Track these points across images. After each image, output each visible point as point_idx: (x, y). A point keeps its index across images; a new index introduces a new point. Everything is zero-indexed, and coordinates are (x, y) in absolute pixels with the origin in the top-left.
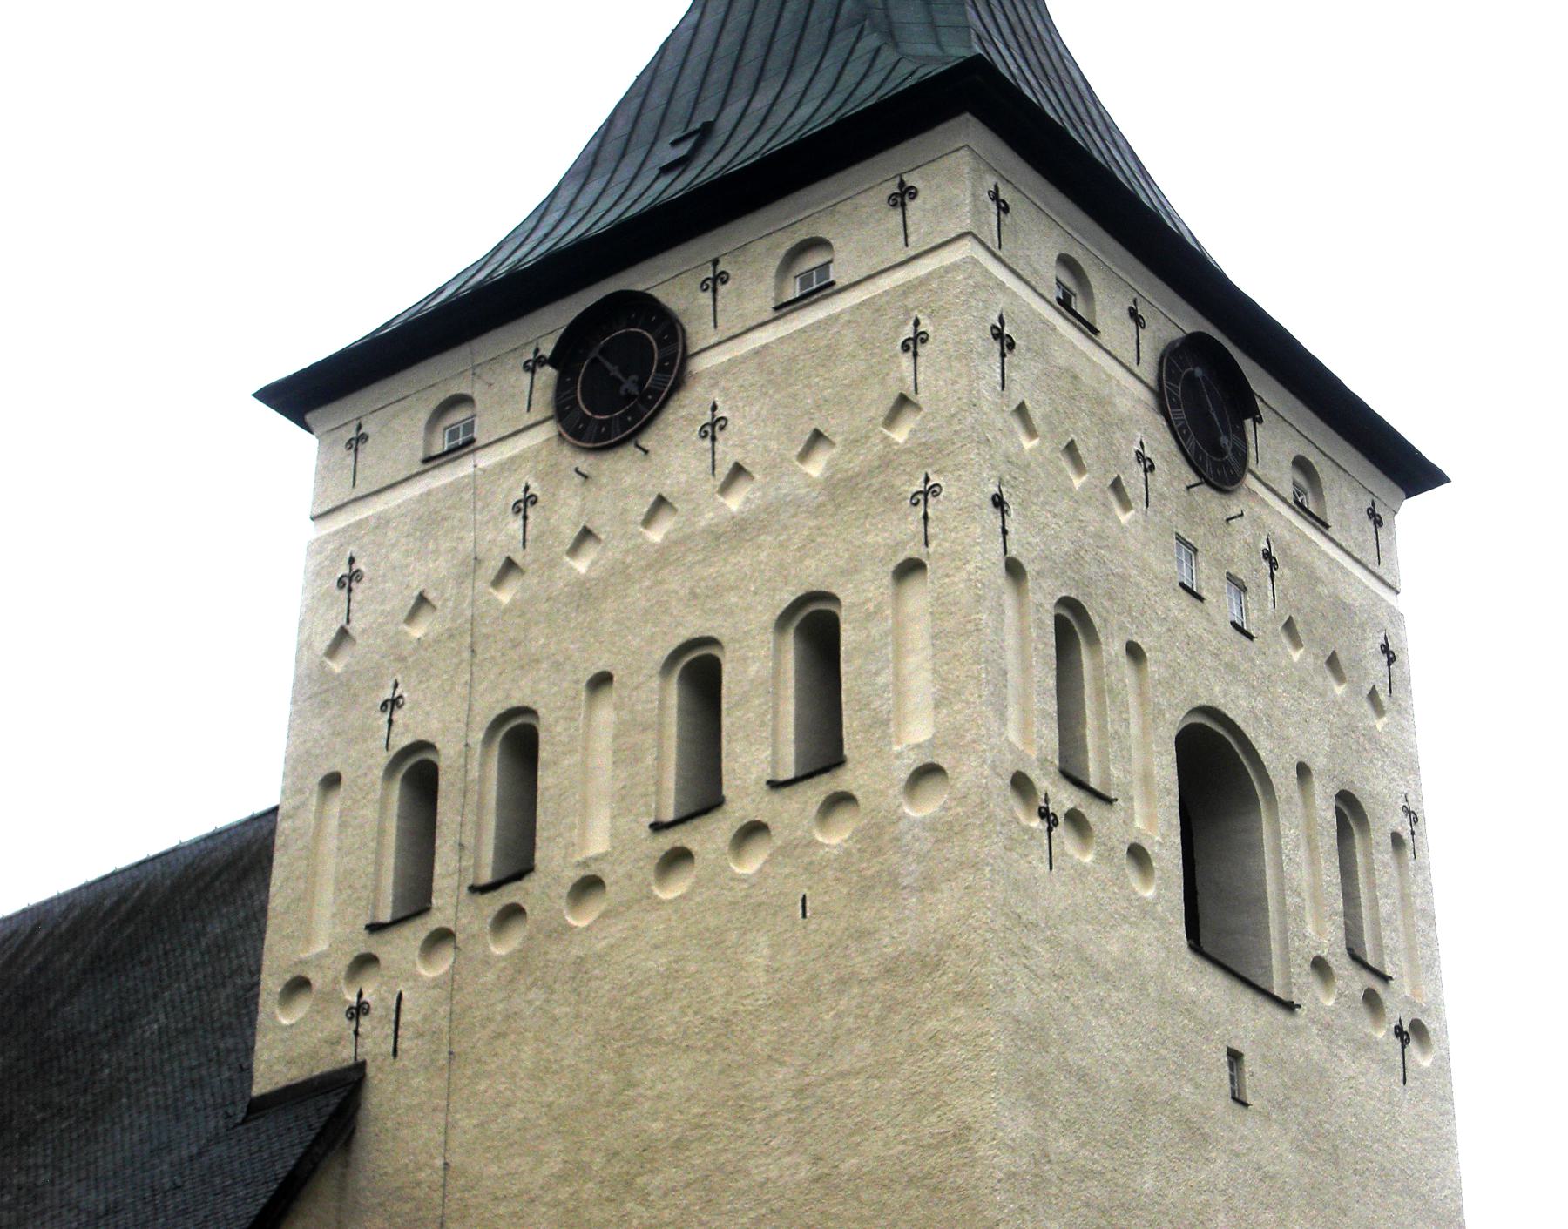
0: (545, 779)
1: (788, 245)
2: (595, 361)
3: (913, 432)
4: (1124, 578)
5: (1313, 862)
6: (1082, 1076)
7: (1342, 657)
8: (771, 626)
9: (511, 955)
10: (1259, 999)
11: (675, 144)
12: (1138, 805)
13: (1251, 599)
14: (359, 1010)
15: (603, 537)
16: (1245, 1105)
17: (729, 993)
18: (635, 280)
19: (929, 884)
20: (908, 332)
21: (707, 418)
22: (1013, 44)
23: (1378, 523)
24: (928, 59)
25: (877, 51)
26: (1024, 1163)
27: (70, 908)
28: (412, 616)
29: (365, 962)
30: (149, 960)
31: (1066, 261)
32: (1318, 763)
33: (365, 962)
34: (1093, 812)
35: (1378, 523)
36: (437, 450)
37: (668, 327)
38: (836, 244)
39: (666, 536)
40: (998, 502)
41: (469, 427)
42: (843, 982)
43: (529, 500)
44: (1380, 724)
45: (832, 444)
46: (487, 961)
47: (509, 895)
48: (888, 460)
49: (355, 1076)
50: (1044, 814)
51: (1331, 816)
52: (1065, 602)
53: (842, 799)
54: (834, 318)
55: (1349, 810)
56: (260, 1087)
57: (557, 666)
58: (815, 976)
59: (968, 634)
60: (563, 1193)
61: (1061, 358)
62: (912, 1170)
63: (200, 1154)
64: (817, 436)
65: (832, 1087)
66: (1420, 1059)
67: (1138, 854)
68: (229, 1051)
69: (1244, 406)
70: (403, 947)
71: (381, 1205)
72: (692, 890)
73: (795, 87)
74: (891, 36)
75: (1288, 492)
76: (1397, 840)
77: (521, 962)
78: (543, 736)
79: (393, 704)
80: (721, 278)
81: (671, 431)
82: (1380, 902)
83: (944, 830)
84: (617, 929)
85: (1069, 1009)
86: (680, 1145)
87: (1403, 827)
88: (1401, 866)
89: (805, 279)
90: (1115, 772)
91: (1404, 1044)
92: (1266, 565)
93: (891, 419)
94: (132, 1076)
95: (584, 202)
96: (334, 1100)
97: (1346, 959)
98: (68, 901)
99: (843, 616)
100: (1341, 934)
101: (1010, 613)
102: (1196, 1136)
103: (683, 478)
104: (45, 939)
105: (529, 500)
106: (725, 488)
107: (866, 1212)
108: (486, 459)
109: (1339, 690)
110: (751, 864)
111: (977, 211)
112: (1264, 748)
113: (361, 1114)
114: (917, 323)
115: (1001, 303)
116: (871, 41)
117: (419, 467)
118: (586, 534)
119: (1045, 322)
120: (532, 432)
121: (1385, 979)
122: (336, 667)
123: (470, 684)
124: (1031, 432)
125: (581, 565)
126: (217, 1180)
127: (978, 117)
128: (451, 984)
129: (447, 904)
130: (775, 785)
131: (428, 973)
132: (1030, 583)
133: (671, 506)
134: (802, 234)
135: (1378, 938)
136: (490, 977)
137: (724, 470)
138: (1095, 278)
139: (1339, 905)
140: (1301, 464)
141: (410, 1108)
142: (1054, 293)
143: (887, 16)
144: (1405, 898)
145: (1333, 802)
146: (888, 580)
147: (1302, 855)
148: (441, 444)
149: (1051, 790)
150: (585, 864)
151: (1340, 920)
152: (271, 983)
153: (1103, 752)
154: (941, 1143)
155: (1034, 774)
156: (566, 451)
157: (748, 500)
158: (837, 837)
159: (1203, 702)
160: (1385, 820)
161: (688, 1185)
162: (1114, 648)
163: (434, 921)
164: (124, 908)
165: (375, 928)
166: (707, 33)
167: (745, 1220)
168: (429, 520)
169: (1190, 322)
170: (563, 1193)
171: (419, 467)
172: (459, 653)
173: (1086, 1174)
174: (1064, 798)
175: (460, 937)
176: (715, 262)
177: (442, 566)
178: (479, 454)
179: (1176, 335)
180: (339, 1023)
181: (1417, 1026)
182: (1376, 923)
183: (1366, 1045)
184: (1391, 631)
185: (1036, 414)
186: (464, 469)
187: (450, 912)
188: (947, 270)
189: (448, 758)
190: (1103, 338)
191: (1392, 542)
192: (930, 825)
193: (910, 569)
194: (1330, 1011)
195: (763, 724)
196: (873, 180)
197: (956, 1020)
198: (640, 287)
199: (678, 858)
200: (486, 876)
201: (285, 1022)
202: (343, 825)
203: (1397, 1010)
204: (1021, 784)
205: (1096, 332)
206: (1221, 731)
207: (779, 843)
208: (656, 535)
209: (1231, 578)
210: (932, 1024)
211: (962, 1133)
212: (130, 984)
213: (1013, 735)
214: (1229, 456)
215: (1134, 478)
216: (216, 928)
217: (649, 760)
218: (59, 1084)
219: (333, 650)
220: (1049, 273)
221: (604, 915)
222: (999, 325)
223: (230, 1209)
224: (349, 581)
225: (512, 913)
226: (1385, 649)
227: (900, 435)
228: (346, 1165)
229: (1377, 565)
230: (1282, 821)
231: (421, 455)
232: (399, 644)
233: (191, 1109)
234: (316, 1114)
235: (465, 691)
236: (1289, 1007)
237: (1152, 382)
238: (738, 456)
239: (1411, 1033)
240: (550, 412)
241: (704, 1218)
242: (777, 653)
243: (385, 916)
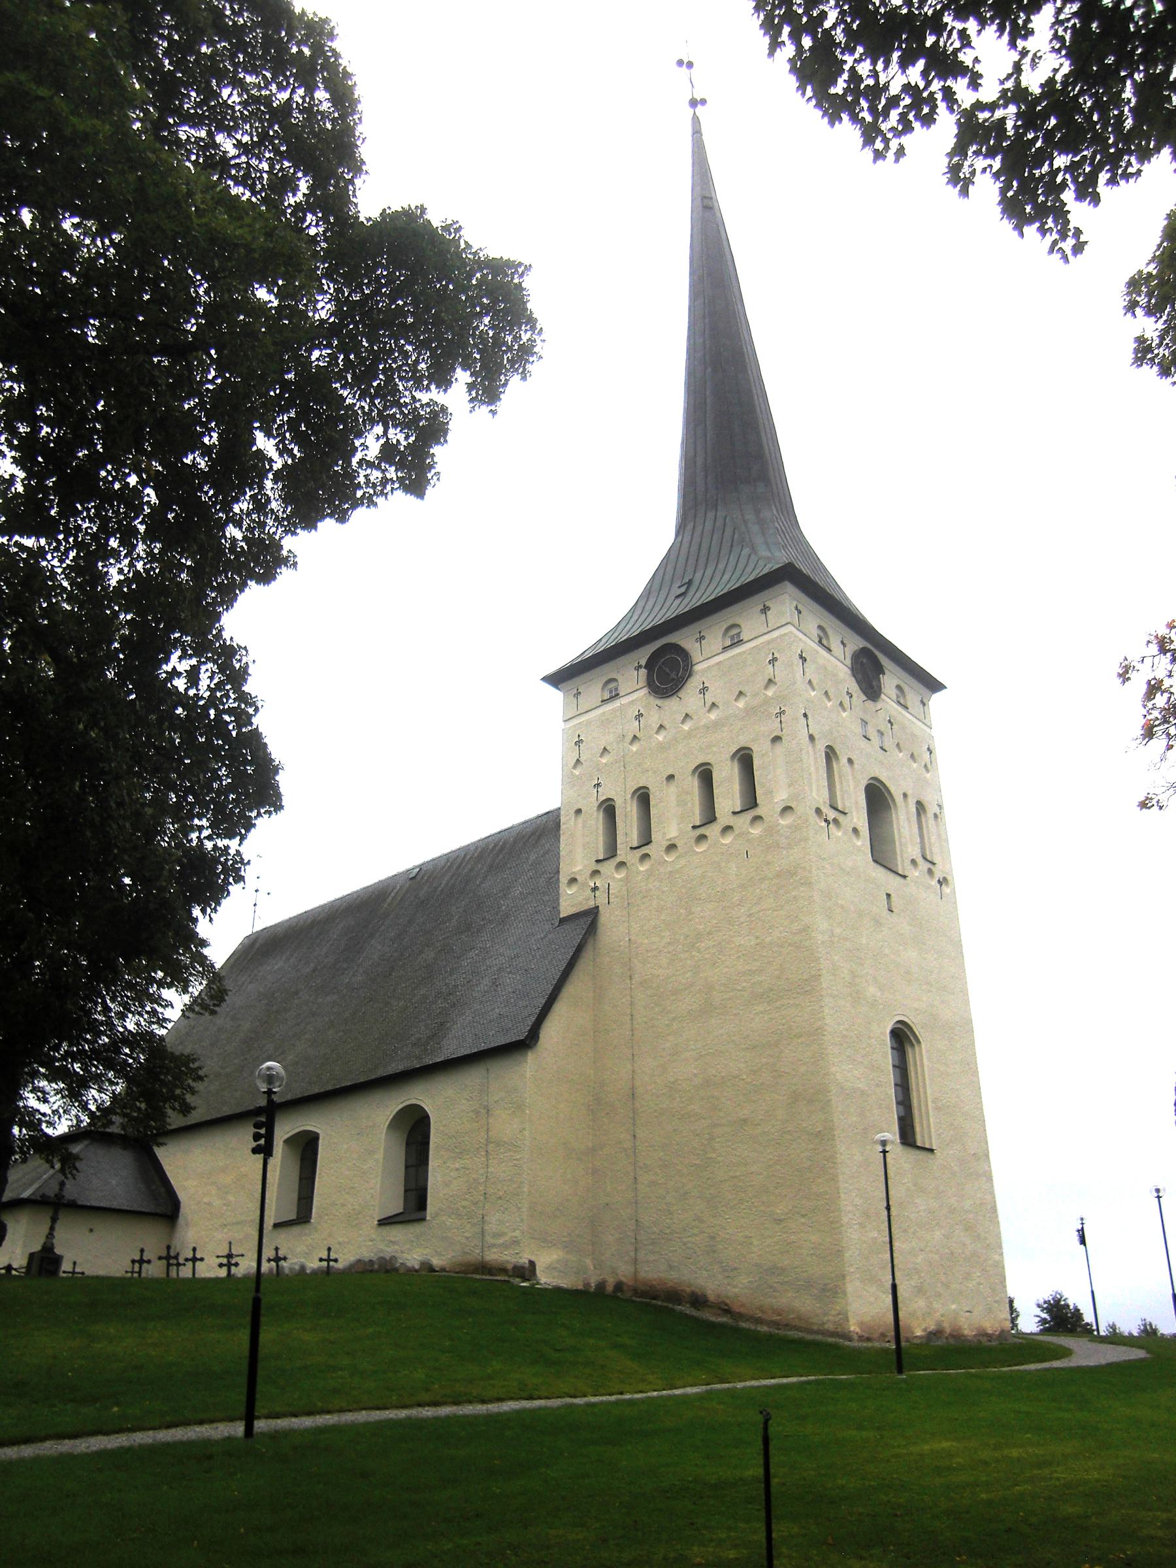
0: (653, 811)
2: (660, 667)
3: (775, 692)
4: (846, 736)
5: (910, 826)
6: (842, 907)
7: (915, 754)
8: (729, 759)
9: (647, 870)
11: (679, 587)
12: (854, 814)
13: (885, 738)
14: (595, 889)
15: (667, 727)
16: (892, 911)
17: (723, 883)
18: (672, 638)
19: (789, 846)
20: (770, 657)
21: (701, 687)
22: (792, 545)
23: (924, 704)
24: (769, 560)
25: (750, 555)
26: (826, 938)
27: (477, 848)
28: (602, 755)
29: (595, 873)
30: (511, 868)
31: (820, 627)
32: (909, 793)
33: (595, 873)
34: (841, 818)
35: (924, 704)
36: (605, 698)
37: (685, 654)
38: (742, 626)
39: (690, 728)
40: (805, 715)
41: (616, 689)
42: (762, 880)
43: (640, 715)
44: (928, 775)
45: (746, 696)
46: (639, 873)
47: (645, 850)
48: (767, 701)
50: (826, 820)
51: (914, 810)
52: (828, 747)
53: (757, 818)
55: (920, 807)
56: (561, 916)
57: (655, 772)
58: (752, 878)
59: (799, 762)
60: (671, 948)
61: (821, 661)
62: (789, 941)
63: (545, 937)
64: (741, 693)
65: (761, 914)
66: (947, 890)
67: (855, 830)
68: (547, 901)
69: (880, 670)
70: (608, 868)
72: (708, 848)
73: (721, 566)
74: (754, 550)
75: (894, 697)
77: (650, 873)
78: (651, 796)
79: (598, 785)
80: (702, 638)
81: (689, 691)
83: (795, 828)
84: (683, 862)
85: (837, 885)
86: (709, 933)
87: (937, 810)
88: (937, 825)
89: (732, 638)
90: (847, 804)
91: (941, 885)
92: (889, 725)
93: (766, 687)
94: (514, 909)
95: (648, 607)
96: (590, 920)
97: (922, 859)
98: (476, 845)
99: (754, 756)
100: (919, 850)
101: (811, 752)
102: (878, 923)
103: (695, 708)
104: (470, 859)
105: (640, 715)
106: (709, 711)
107: (775, 955)
108: (624, 701)
109: (915, 765)
110: (727, 840)
111: (791, 615)
112: (892, 789)
113: (598, 923)
114: (773, 654)
115: (801, 646)
116: (746, 551)
117: (600, 704)
119: (815, 650)
120: (638, 692)
121: (934, 864)
122: (577, 772)
123: (625, 779)
124: (814, 689)
125: (660, 738)
126: (553, 946)
128: (627, 880)
129: (623, 853)
130: (734, 813)
131: (618, 876)
132: (817, 742)
133: (691, 717)
134: (730, 622)
135: (931, 850)
136: (639, 878)
137: (708, 704)
138: (830, 632)
139: (918, 841)
140: (899, 687)
141: (615, 921)
142: (817, 640)
143: (751, 541)
144: (939, 836)
145: (915, 806)
146: (769, 743)
147: (906, 824)
148: (607, 696)
149: (827, 812)
150: (670, 840)
151: (919, 846)
152: (563, 879)
153: (843, 799)
154: (800, 932)
155: (822, 808)
156: (652, 698)
157: (718, 715)
158: (756, 831)
159: (872, 776)
160: (931, 809)
161: (714, 946)
162: (844, 761)
163: (618, 859)
164: (497, 848)
165: (598, 861)
166: (686, 545)
168: (605, 722)
169: (861, 643)
171: (600, 704)
172: (619, 768)
173: (846, 939)
174: (832, 815)
175: (628, 865)
176: (700, 632)
177: (611, 738)
178: (621, 699)
179: (856, 648)
180: (588, 892)
181: (945, 879)
182: (930, 844)
183: (929, 887)
184: (931, 742)
185: (815, 682)
186: (617, 704)
187: (624, 855)
188: (783, 635)
189: (619, 804)
192: (789, 827)
193: (777, 739)
194: (917, 877)
195: (729, 793)
196: (755, 602)
197: (803, 892)
198: (673, 641)
199: (702, 838)
200: (635, 844)
201: (569, 892)
202: (584, 826)
203: (938, 875)
204: (818, 811)
205: (831, 651)
206: (878, 785)
207: (737, 833)
208: (686, 727)
209: (878, 731)
211: (806, 929)
212: (506, 876)
213: (814, 794)
214: (875, 687)
216: (533, 857)
217: (689, 805)
218: (487, 912)
219: (575, 767)
220: (815, 632)
221: (677, 858)
223: (560, 957)
224: (579, 742)
225: (646, 856)
226: (929, 749)
227: (770, 693)
228: (595, 940)
229: (924, 719)
230: (899, 813)
231: (600, 699)
232: (598, 765)
233: (538, 922)
234: (584, 923)
236: (905, 877)
237: (850, 666)
238: (714, 700)
239: (943, 882)
240: (645, 684)
241: (720, 957)
242: (732, 769)
243: (601, 857)
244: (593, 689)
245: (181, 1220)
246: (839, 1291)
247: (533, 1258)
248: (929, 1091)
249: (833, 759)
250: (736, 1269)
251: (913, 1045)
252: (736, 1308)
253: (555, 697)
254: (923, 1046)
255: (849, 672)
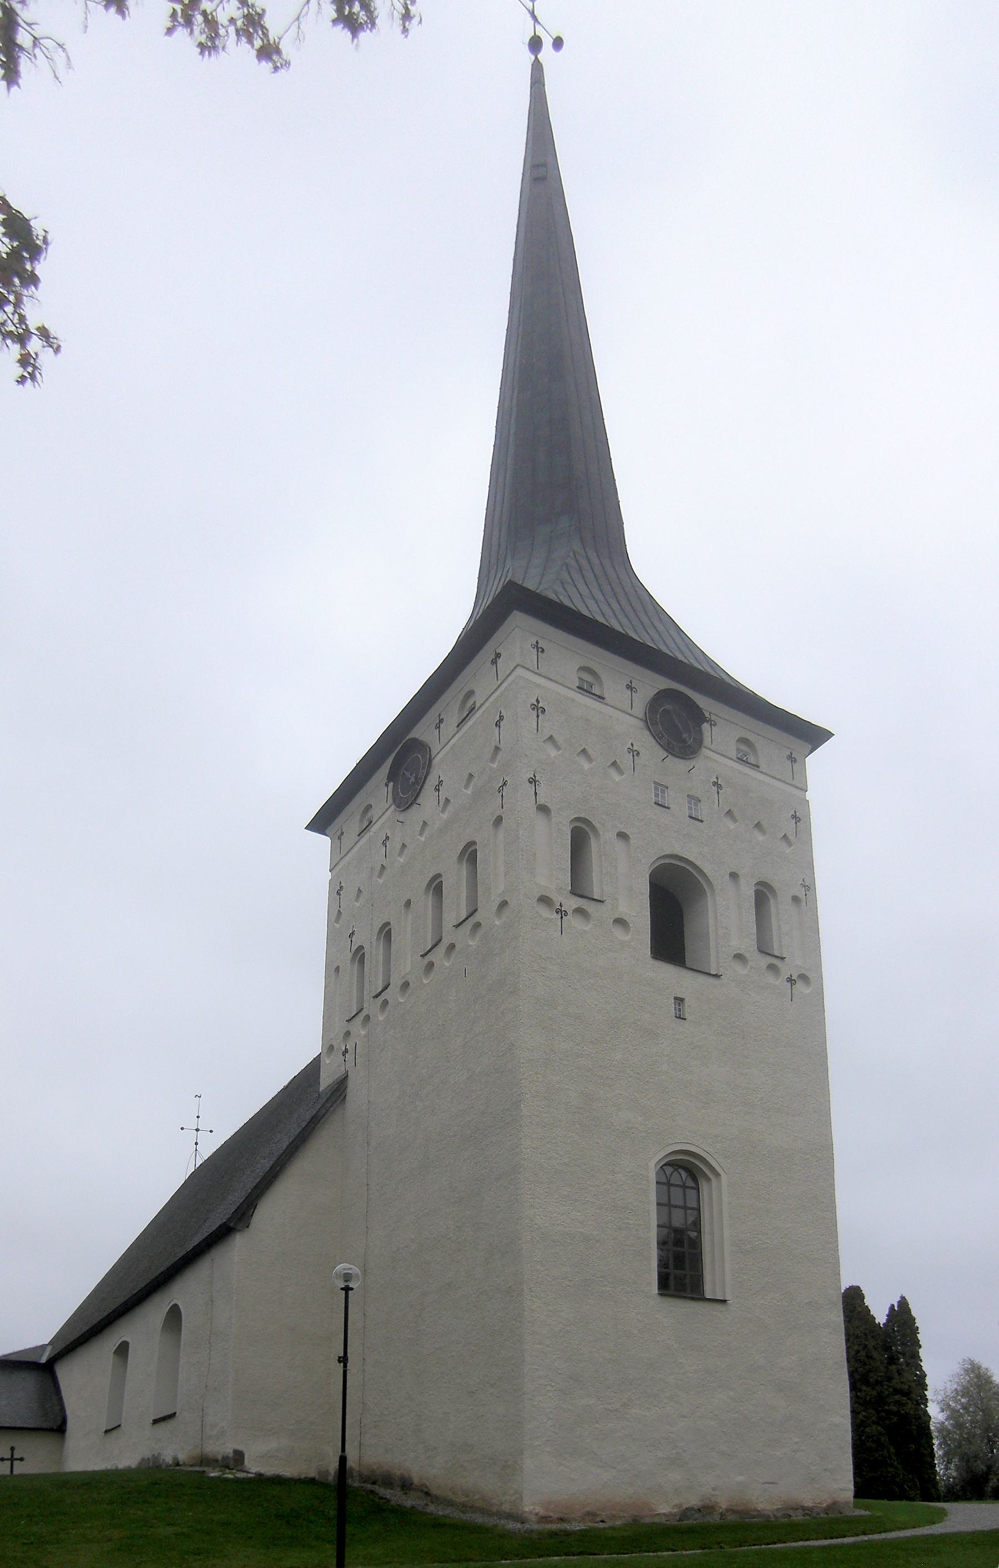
1: (461, 697)
10: (696, 975)
33: (348, 1034)
70: (357, 1025)
71: (353, 1120)
76: (796, 899)
82: (782, 926)
87: (801, 893)
118: (404, 846)
127: (521, 611)
167: (449, 1099)
171: (358, 838)
185: (560, 739)
190: (608, 700)
205: (603, 698)
206: (683, 865)
215: (626, 761)
222: (536, 704)
244: (350, 820)
245: (68, 1433)
246: (518, 1467)
247: (240, 1448)
248: (727, 1233)
249: (591, 836)
250: (435, 1448)
251: (709, 1180)
252: (434, 1491)
253: (323, 842)
254: (724, 1177)
255: (640, 724)
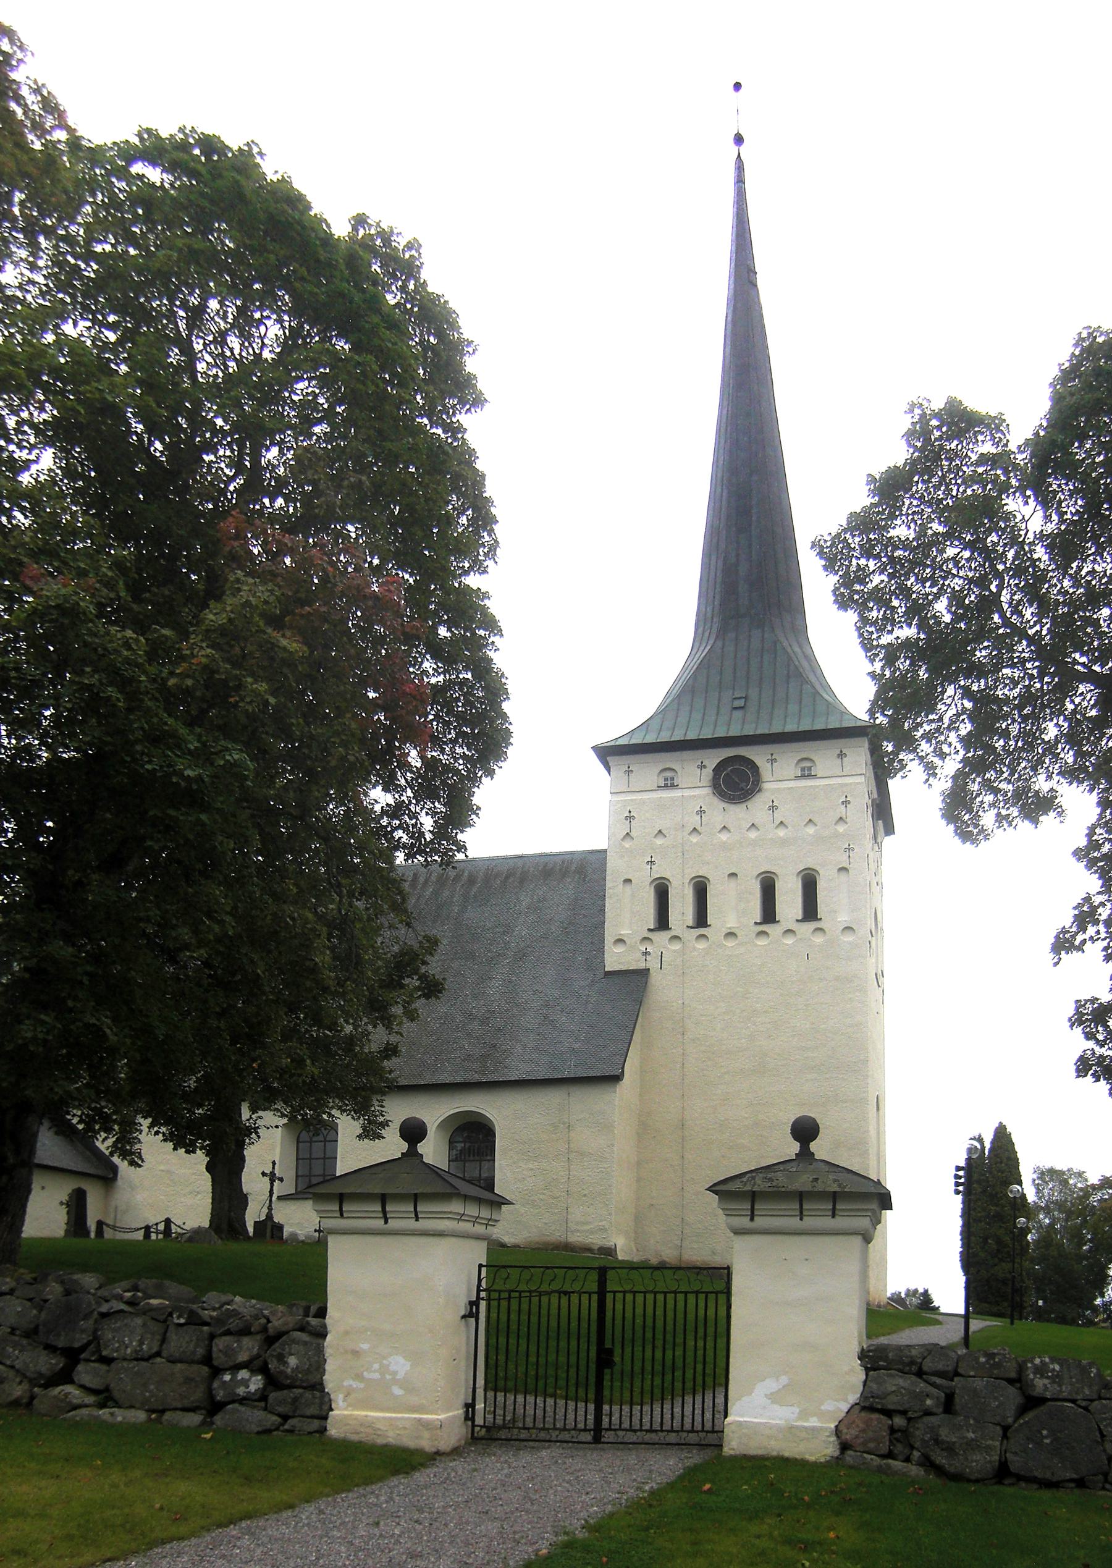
37: (755, 768)
46: (694, 949)
49: (645, 972)
54: (817, 787)
60: (726, 1017)
84: (742, 950)
117: (793, 778)
170: (726, 1017)
191: (469, 1290)
210: (850, 996)
224: (630, 818)
235: (681, 866)
